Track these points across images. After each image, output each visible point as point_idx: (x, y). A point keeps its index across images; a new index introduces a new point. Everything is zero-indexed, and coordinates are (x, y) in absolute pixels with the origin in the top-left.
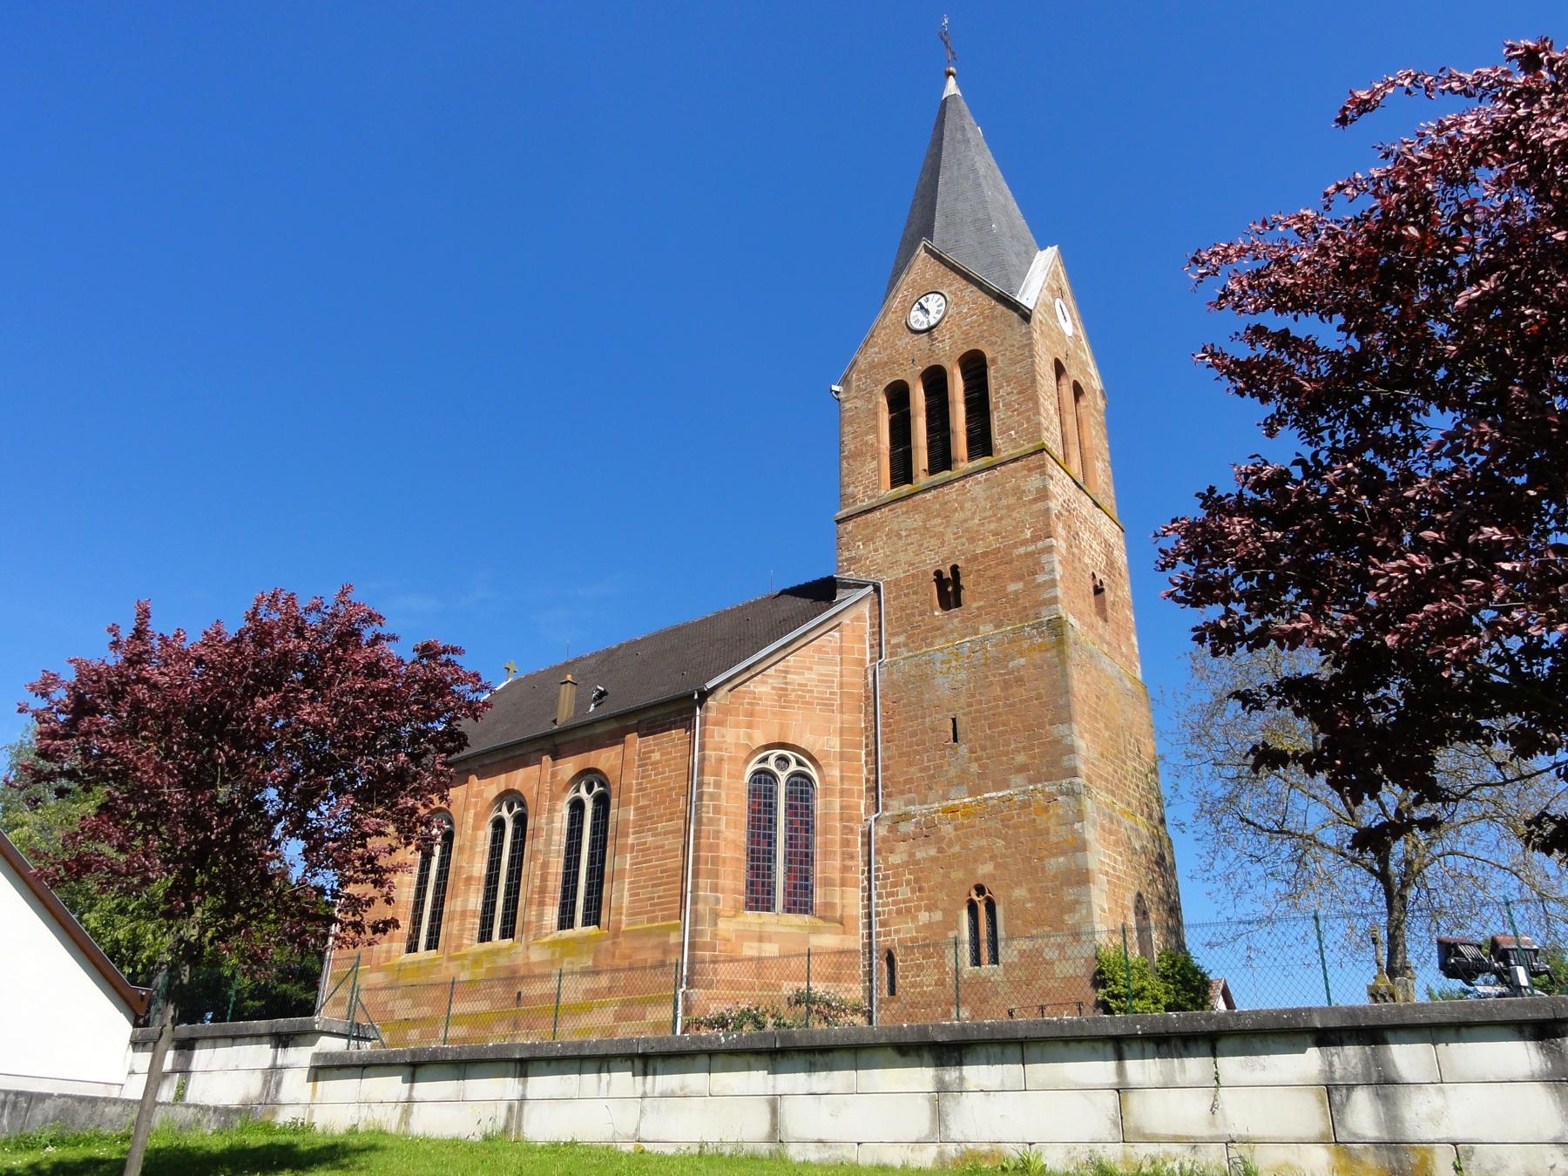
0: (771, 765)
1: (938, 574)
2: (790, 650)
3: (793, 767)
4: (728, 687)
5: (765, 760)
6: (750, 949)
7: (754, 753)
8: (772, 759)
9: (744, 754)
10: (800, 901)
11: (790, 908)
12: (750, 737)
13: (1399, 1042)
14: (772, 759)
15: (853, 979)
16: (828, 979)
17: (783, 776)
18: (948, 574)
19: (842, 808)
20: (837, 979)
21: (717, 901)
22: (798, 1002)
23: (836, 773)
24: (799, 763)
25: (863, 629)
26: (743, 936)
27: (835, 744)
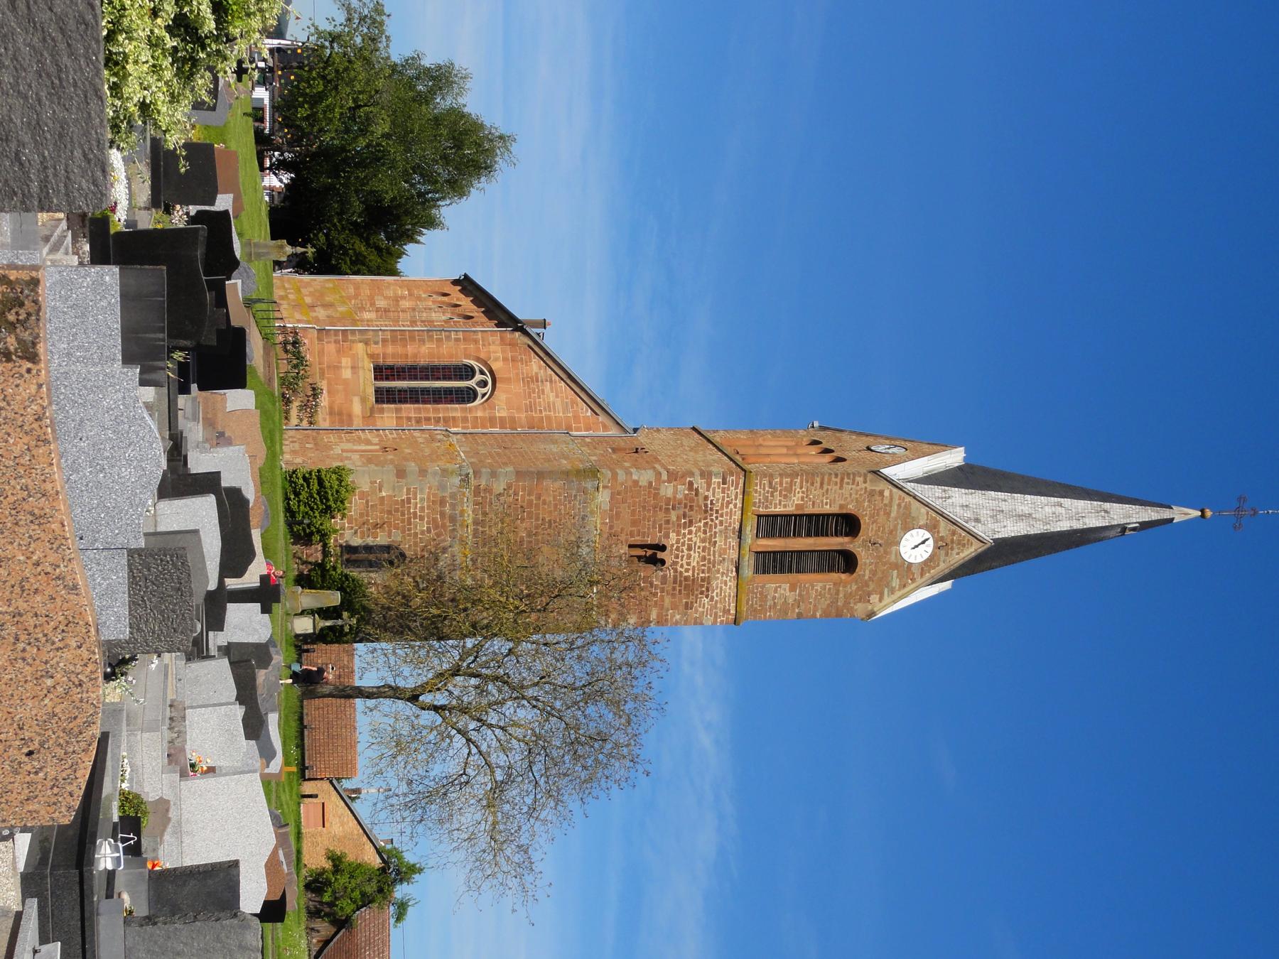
0: (478, 377)
1: (663, 548)
2: (569, 381)
3: (480, 391)
4: (531, 343)
5: (482, 373)
6: (346, 362)
7: (485, 364)
8: (483, 377)
9: (482, 356)
10: (384, 396)
11: (378, 391)
12: (496, 359)
13: (128, 298)
14: (483, 377)
15: (332, 422)
16: (331, 408)
17: (472, 383)
18: (660, 555)
19: (454, 418)
20: (331, 413)
21: (376, 343)
22: (314, 389)
23: (479, 414)
24: (484, 395)
25: (598, 430)
26: (354, 357)
27: (501, 412)
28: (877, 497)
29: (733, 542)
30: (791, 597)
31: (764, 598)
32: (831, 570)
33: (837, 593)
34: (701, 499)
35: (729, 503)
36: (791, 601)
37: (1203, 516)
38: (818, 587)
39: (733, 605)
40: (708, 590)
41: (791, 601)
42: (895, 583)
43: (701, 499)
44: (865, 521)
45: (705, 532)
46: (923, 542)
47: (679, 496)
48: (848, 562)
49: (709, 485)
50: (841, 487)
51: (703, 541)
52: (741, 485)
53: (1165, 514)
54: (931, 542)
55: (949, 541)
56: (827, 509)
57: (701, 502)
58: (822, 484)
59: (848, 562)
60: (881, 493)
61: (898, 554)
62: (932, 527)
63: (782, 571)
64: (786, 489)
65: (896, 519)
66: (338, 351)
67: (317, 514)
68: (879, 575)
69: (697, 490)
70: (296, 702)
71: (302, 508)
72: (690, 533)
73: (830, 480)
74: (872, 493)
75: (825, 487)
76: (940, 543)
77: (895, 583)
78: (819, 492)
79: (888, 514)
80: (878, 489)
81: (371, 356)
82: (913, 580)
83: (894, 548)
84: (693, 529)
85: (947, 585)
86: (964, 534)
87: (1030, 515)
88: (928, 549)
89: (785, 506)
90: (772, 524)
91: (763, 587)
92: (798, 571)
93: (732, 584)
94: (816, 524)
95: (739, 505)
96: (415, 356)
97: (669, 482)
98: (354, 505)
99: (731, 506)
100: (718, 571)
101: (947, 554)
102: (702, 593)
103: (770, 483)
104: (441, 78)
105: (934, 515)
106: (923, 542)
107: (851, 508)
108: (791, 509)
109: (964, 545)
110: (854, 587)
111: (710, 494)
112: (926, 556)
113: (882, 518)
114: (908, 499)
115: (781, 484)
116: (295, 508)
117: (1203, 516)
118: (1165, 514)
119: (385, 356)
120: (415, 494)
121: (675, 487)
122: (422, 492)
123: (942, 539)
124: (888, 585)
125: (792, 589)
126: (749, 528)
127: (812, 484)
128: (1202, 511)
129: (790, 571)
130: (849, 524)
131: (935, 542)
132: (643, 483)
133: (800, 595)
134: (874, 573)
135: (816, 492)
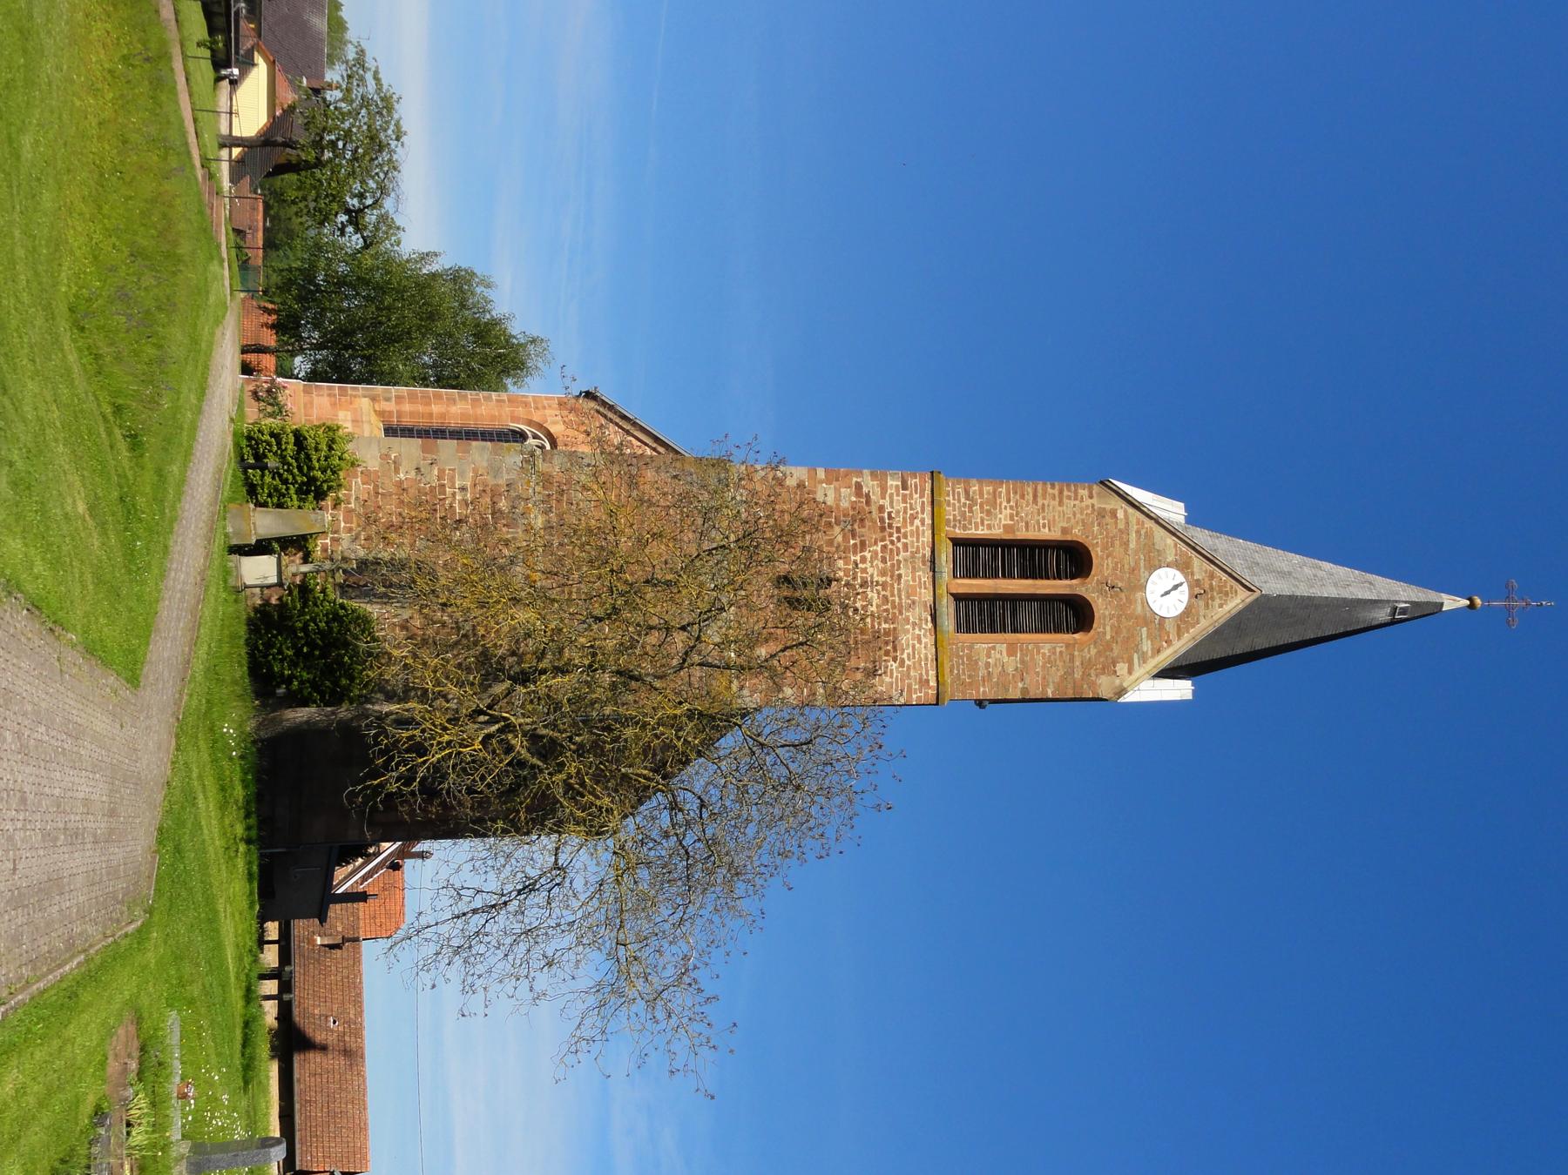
5: (535, 437)
9: (536, 418)
28: (1108, 519)
29: (925, 576)
30: (1011, 663)
31: (973, 664)
32: (1058, 630)
33: (1072, 659)
34: (874, 509)
35: (913, 517)
36: (1010, 670)
37: (1472, 606)
38: (1046, 649)
39: (932, 673)
40: (895, 649)
41: (1010, 670)
42: (1147, 646)
43: (874, 509)
44: (1097, 553)
45: (884, 560)
46: (1176, 587)
47: (845, 504)
48: (1078, 615)
49: (884, 489)
50: (1061, 503)
51: (883, 573)
52: (928, 492)
53: (1430, 596)
54: (1185, 587)
55: (1207, 586)
56: (1045, 534)
57: (875, 514)
58: (1035, 496)
59: (1078, 615)
60: (1114, 514)
61: (1145, 603)
62: (1183, 566)
63: (993, 631)
64: (988, 502)
65: (1136, 552)
66: (334, 405)
67: (292, 490)
68: (1124, 633)
69: (868, 496)
70: (255, 926)
71: (268, 479)
72: (863, 560)
73: (1045, 492)
74: (1101, 514)
75: (1040, 502)
76: (1197, 590)
77: (1147, 646)
78: (1032, 508)
79: (1126, 544)
80: (1108, 507)
81: (380, 414)
82: (1169, 642)
83: (1139, 595)
84: (868, 555)
85: (1180, 690)
86: (1224, 577)
87: (1290, 573)
88: (1183, 595)
89: (989, 527)
90: (976, 554)
91: (971, 648)
92: (1015, 631)
93: (929, 640)
94: (1030, 556)
95: (928, 521)
96: (443, 416)
97: (829, 482)
98: (355, 489)
99: (917, 522)
100: (907, 620)
101: (1207, 606)
102: (887, 653)
103: (967, 492)
104: (460, 280)
105: (1184, 548)
106: (1176, 587)
107: (1076, 534)
108: (997, 532)
109: (1227, 594)
110: (1093, 651)
111: (886, 502)
112: (1181, 608)
113: (1118, 549)
114: (1149, 524)
115: (981, 495)
116: (256, 480)
117: (1472, 606)
118: (1430, 596)
119: (400, 414)
120: (452, 479)
121: (837, 490)
122: (462, 475)
123: (1198, 583)
124: (1137, 649)
125: (1011, 653)
126: (944, 557)
127: (1023, 497)
128: (1470, 599)
129: (1004, 630)
130: (1075, 558)
131: (1191, 588)
132: (791, 482)
133: (1022, 662)
134: (1117, 631)
135: (1028, 509)
